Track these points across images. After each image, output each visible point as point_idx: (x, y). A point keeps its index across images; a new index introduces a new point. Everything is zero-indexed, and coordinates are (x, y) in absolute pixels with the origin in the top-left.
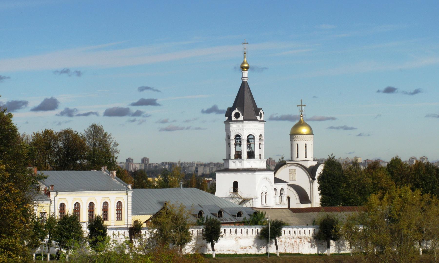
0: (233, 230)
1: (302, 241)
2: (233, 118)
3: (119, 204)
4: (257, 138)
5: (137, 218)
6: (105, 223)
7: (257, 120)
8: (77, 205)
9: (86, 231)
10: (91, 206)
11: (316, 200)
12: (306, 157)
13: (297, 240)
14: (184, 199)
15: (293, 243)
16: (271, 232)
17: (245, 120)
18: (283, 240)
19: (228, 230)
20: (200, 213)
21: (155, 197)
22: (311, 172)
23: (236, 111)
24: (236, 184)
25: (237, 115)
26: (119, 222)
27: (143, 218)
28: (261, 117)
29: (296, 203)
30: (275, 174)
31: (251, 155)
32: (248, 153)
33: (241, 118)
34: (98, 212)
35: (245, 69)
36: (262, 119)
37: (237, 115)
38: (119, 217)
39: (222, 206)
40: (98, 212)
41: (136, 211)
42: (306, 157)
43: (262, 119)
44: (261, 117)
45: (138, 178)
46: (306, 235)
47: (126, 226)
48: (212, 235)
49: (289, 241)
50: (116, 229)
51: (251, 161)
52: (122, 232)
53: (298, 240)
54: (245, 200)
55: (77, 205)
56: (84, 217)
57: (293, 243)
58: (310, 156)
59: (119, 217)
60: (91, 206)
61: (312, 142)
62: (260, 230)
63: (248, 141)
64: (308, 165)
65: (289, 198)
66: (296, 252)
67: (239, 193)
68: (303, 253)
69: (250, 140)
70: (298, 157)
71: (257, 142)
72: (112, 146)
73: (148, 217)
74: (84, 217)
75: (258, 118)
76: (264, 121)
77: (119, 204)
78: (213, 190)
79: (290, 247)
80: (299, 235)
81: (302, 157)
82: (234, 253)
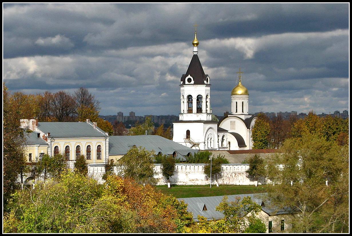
0: (184, 167)
1: (237, 175)
2: (187, 82)
3: (99, 148)
4: (204, 97)
5: (111, 158)
6: (88, 161)
7: (204, 84)
8: (67, 149)
9: (71, 165)
10: (78, 148)
11: (249, 144)
12: (243, 112)
13: (236, 175)
14: (150, 144)
15: (230, 176)
16: (214, 169)
17: (195, 84)
18: (188, 170)
19: (180, 167)
20: (189, 154)
21: (129, 141)
22: (247, 123)
23: (189, 76)
24: (188, 132)
25: (189, 80)
26: (99, 161)
27: (116, 158)
28: (207, 81)
29: (235, 146)
30: (218, 126)
31: (199, 110)
32: (197, 108)
33: (193, 82)
34: (83, 152)
35: (195, 45)
36: (209, 83)
37: (189, 80)
38: (99, 157)
39: (176, 149)
40: (83, 152)
41: (111, 152)
42: (243, 112)
43: (209, 83)
44: (207, 81)
45: (115, 126)
46: (239, 171)
47: (105, 163)
48: (169, 172)
49: (226, 175)
50: (96, 166)
51: (190, 115)
52: (100, 168)
53: (233, 175)
54: (194, 145)
55: (67, 149)
56: (73, 156)
57: (230, 176)
58: (246, 111)
59: (99, 157)
60: (78, 148)
61: (247, 101)
62: (203, 166)
63: (198, 100)
64: (243, 117)
65: (229, 143)
66: (231, 183)
67: (191, 139)
68: (237, 185)
69: (199, 99)
70: (237, 112)
71: (204, 100)
72: (95, 104)
73: (119, 157)
74: (73, 156)
75: (205, 82)
76: (210, 85)
77: (99, 148)
78: (170, 136)
79: (227, 179)
80: (234, 171)
81: (240, 111)
82: (184, 184)
